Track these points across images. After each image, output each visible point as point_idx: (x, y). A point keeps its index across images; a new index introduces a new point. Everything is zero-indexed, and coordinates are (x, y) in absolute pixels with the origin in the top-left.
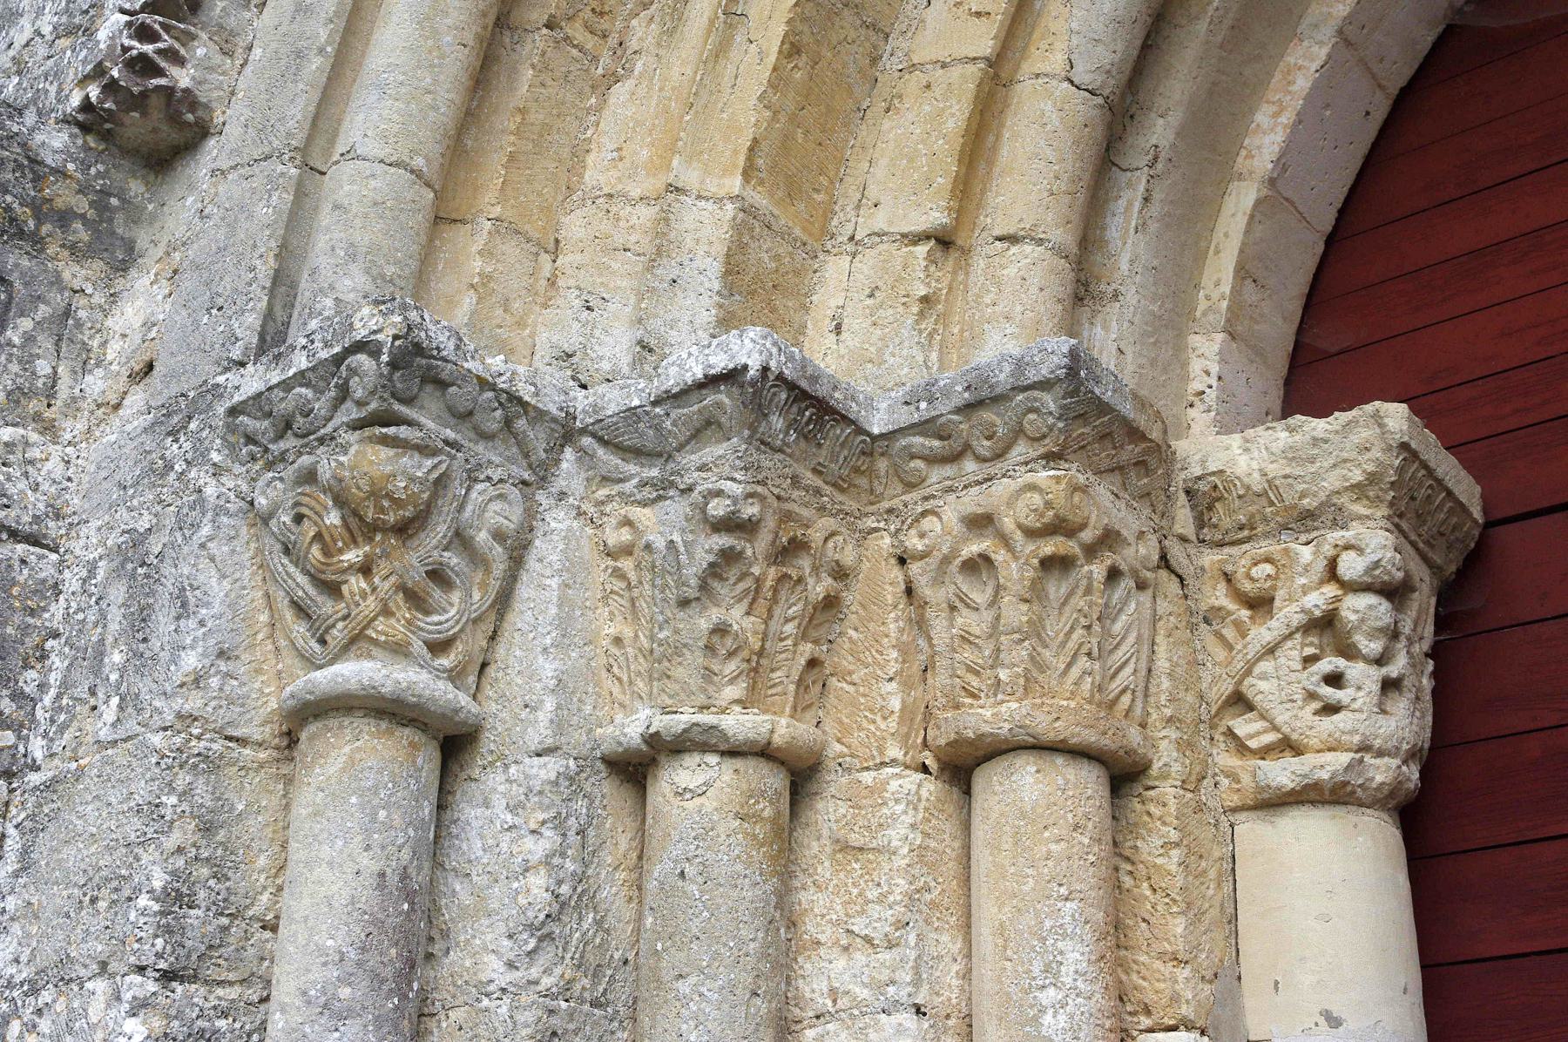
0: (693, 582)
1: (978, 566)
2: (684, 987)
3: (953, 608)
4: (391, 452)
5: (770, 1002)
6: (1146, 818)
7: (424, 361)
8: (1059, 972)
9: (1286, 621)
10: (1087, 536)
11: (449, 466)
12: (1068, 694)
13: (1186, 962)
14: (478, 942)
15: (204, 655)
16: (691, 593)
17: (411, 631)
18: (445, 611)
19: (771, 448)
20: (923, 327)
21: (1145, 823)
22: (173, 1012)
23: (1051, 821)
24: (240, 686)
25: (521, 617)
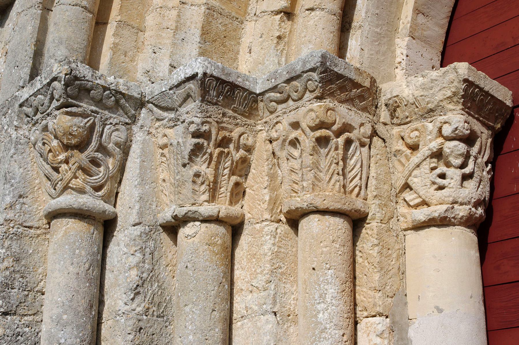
0: (187, 157)
1: (294, 143)
2: (187, 309)
3: (288, 159)
4: (70, 118)
5: (220, 313)
6: (367, 235)
7: (79, 82)
8: (326, 297)
9: (423, 154)
10: (335, 128)
11: (94, 121)
12: (330, 190)
13: (380, 291)
14: (116, 296)
15: (13, 197)
16: (186, 161)
17: (85, 183)
18: (98, 175)
19: (212, 104)
20: (278, 48)
21: (366, 237)
22: (7, 326)
23: (323, 240)
24: (28, 207)
25: (127, 175)
